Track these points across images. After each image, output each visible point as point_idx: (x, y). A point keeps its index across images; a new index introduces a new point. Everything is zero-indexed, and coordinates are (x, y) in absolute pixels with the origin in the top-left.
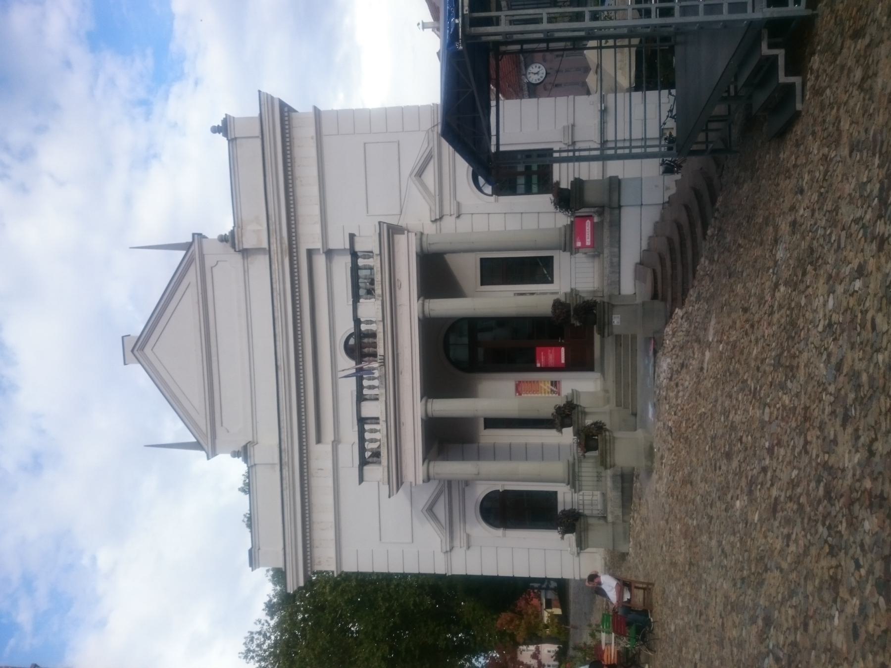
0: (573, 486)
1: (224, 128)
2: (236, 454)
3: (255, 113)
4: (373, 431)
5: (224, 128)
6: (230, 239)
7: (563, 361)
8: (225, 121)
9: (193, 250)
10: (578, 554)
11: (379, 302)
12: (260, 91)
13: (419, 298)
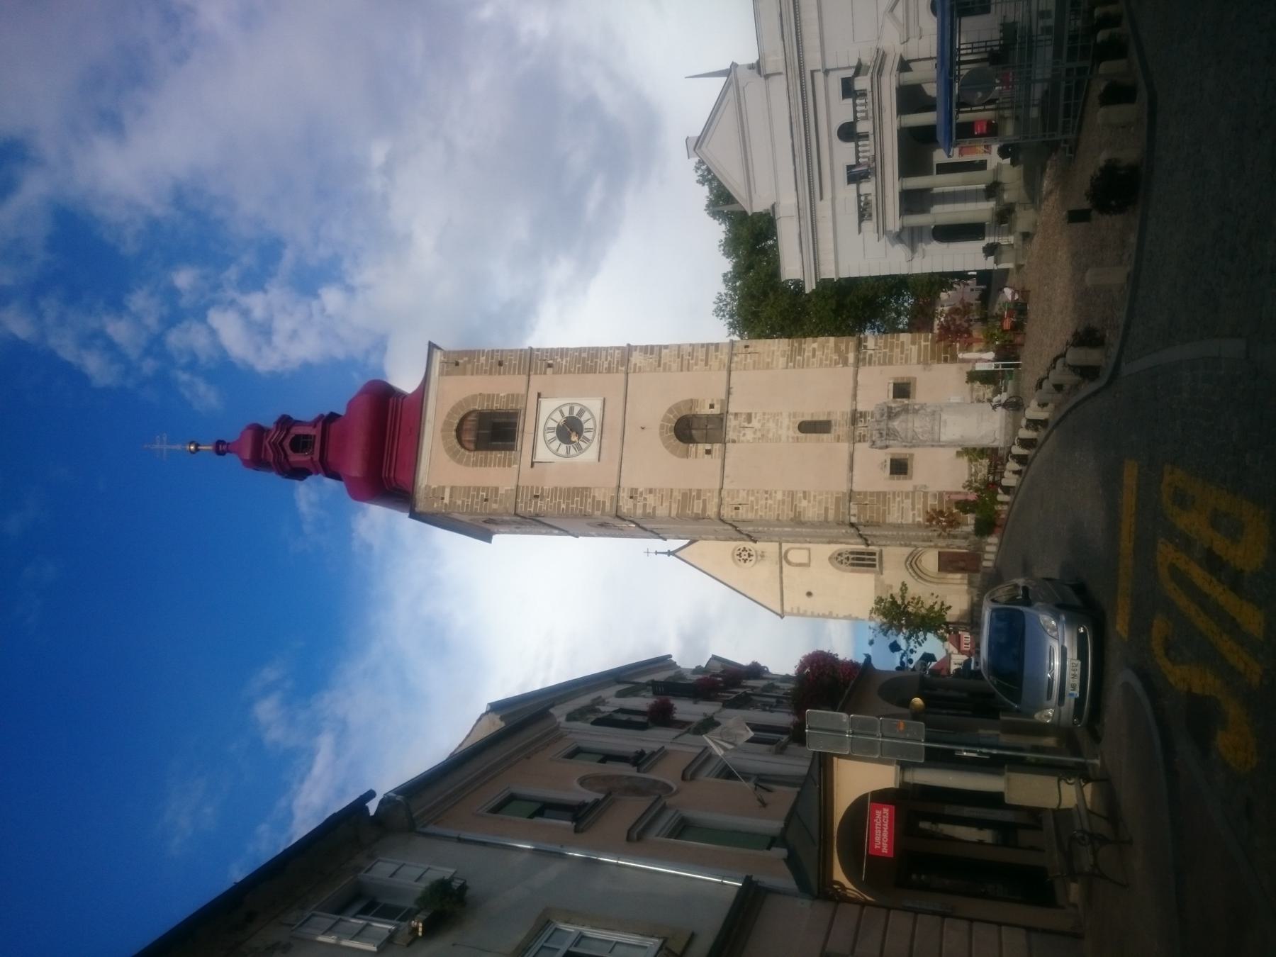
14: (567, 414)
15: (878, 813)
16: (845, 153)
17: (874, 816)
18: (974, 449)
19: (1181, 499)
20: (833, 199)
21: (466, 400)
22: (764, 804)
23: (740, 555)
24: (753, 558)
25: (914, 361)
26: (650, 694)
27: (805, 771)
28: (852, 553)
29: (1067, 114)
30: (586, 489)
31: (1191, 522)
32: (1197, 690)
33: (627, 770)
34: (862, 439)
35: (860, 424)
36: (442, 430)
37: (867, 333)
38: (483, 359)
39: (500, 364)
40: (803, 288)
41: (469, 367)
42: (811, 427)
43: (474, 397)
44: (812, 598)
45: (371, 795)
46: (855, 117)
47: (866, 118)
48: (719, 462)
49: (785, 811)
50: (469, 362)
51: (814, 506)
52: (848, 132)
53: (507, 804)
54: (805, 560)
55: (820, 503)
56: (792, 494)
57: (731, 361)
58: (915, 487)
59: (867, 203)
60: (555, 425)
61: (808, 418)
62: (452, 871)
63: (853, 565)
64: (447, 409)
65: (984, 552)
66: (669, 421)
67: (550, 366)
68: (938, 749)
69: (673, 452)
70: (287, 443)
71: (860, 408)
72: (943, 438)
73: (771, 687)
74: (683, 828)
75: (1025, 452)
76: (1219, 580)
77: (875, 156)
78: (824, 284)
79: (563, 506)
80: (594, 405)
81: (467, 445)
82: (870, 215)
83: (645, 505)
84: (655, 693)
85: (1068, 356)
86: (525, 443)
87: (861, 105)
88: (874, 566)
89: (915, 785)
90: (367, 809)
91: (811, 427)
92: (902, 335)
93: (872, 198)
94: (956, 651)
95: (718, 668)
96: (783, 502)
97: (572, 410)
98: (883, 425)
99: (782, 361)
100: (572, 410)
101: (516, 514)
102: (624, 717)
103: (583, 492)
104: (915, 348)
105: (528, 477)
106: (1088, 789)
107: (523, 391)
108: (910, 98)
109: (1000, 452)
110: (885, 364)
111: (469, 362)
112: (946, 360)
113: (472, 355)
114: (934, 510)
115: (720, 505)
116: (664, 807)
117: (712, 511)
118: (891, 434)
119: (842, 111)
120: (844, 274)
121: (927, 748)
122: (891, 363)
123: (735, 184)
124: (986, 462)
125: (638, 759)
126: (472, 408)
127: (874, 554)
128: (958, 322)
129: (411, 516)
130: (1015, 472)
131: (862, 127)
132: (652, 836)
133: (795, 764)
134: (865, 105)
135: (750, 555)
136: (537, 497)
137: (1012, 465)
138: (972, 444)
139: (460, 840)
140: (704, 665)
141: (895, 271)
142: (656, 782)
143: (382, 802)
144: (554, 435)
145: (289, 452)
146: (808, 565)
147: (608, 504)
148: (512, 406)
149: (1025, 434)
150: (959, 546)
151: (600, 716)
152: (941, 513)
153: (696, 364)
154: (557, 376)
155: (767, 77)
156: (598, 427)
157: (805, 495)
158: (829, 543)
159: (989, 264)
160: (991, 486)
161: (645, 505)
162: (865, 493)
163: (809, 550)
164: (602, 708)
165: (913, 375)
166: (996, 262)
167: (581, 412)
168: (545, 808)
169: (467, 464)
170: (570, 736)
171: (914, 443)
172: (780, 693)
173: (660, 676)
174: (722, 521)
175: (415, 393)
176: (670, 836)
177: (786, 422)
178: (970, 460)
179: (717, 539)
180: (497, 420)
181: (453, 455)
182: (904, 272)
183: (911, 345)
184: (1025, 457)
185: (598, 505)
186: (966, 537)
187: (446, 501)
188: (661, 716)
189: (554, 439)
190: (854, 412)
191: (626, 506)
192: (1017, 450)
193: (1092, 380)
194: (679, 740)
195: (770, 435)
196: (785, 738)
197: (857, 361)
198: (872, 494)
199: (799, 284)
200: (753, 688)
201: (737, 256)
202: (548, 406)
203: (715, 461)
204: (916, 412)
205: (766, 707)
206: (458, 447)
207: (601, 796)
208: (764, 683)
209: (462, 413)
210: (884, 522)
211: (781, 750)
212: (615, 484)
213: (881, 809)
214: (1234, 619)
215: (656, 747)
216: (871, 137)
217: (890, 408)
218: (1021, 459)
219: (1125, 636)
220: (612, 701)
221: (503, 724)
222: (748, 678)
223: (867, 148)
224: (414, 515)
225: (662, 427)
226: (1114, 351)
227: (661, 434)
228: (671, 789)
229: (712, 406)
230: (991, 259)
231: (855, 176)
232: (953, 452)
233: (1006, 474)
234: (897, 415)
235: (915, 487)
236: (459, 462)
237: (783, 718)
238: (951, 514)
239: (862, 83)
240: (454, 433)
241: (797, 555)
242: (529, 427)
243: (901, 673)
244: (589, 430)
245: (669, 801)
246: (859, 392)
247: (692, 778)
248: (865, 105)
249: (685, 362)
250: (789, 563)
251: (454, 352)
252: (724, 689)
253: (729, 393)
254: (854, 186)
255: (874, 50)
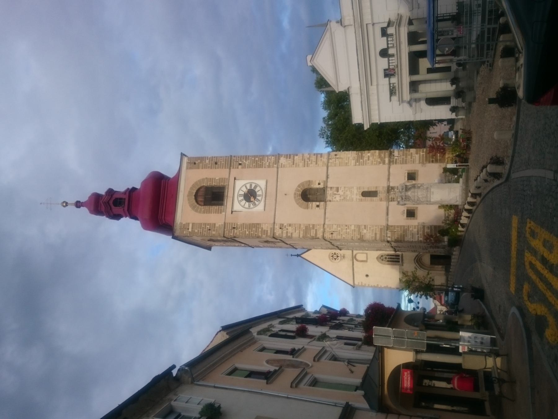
4: (392, 60)
10: (491, 101)
11: (395, 49)
14: (249, 188)
15: (406, 373)
16: (383, 63)
17: (404, 375)
18: (447, 205)
19: (533, 234)
20: (377, 85)
21: (199, 181)
22: (352, 372)
23: (333, 256)
24: (339, 258)
25: (418, 162)
26: (295, 323)
27: (371, 357)
28: (388, 255)
29: (488, 49)
30: (258, 224)
31: (536, 244)
32: (539, 313)
33: (289, 357)
34: (393, 200)
35: (392, 193)
36: (188, 196)
37: (394, 147)
38: (207, 161)
39: (216, 163)
40: (363, 128)
41: (201, 165)
42: (366, 194)
43: (203, 180)
44: (368, 278)
45: (174, 367)
46: (388, 46)
47: (393, 47)
48: (323, 211)
49: (362, 375)
50: (201, 162)
51: (369, 233)
52: (384, 53)
53: (233, 372)
54: (365, 259)
55: (373, 230)
56: (359, 227)
57: (328, 162)
58: (419, 223)
59: (394, 87)
60: (243, 193)
61: (366, 190)
62: (214, 400)
63: (388, 261)
64: (190, 186)
65: (452, 254)
66: (298, 191)
67: (240, 164)
68: (432, 344)
69: (301, 206)
70: (111, 202)
71: (392, 185)
72: (432, 200)
73: (351, 320)
74: (315, 383)
75: (471, 208)
76: (546, 268)
77: (397, 65)
78: (373, 125)
79: (247, 233)
80: (262, 183)
81: (200, 203)
82: (395, 93)
83: (287, 232)
84: (297, 323)
85: (488, 168)
86: (228, 202)
87: (391, 41)
88: (399, 262)
89: (422, 360)
90: (172, 373)
91: (366, 194)
92: (411, 149)
93: (396, 85)
94: (439, 304)
95: (325, 311)
96: (355, 230)
97: (251, 185)
98: (403, 194)
99: (353, 162)
100: (251, 185)
101: (224, 237)
102: (284, 333)
103: (256, 226)
104: (417, 156)
105: (230, 219)
106: (499, 360)
107: (227, 177)
108: (413, 38)
109: (460, 207)
110: (403, 163)
111: (201, 162)
112: (433, 162)
113: (202, 159)
114: (428, 235)
115: (324, 232)
116: (306, 374)
117: (320, 235)
118: (407, 198)
119: (382, 43)
120: (383, 121)
121: (428, 344)
122: (406, 163)
123: (329, 75)
124: (453, 211)
125: (293, 352)
126: (202, 185)
127: (398, 256)
128: (438, 144)
129: (173, 238)
130: (466, 217)
131: (391, 51)
132: (302, 385)
133: (367, 354)
134: (393, 40)
135: (337, 256)
136: (234, 228)
137: (465, 214)
138: (445, 203)
139: (215, 387)
140: (318, 310)
141: (408, 119)
142: (301, 362)
143: (179, 370)
144: (242, 198)
145: (113, 206)
146: (366, 261)
147: (269, 232)
148: (222, 184)
149: (470, 199)
150: (440, 252)
151: (273, 333)
152: (431, 236)
153: (311, 163)
154: (244, 169)
155: (345, 27)
156: (264, 194)
157: (365, 227)
158: (377, 250)
159: (453, 116)
160: (456, 221)
161: (287, 232)
162: (394, 226)
163: (367, 254)
164: (273, 329)
165: (416, 169)
166: (456, 115)
167: (256, 187)
168: (252, 374)
169: (200, 212)
170: (260, 342)
171: (419, 202)
172: (356, 323)
173: (299, 315)
174: (326, 240)
175: (174, 177)
176: (310, 386)
177: (355, 191)
178: (445, 210)
179: (322, 248)
180: (214, 191)
181: (194, 208)
182: (412, 120)
183: (416, 154)
184: (471, 210)
185: (264, 232)
186: (444, 247)
187: (190, 230)
188: (302, 333)
189: (242, 200)
190: (389, 187)
191: (278, 232)
192: (467, 207)
193: (499, 179)
194: (310, 344)
195: (348, 198)
196: (360, 343)
197: (390, 162)
198: (398, 226)
199: (361, 126)
200: (343, 320)
201: (330, 110)
202: (240, 184)
203: (320, 211)
204: (419, 187)
205: (350, 329)
206: (196, 204)
207: (277, 368)
208: (348, 318)
209: (198, 187)
210: (404, 241)
211: (359, 348)
212: (272, 222)
213: (407, 371)
214: (551, 284)
215: (301, 347)
216: (396, 56)
217: (406, 186)
218: (469, 211)
219: (513, 292)
220: (277, 326)
221: (228, 337)
222: (340, 316)
223: (394, 61)
224: (175, 237)
225: (295, 194)
226: (507, 167)
227: (295, 197)
228: (309, 365)
229: (319, 184)
230: (454, 114)
231: (388, 74)
232: (437, 206)
233: (462, 218)
234: (410, 189)
235: (419, 223)
236: (196, 211)
237: (359, 334)
238: (436, 237)
239: (391, 30)
240: (194, 197)
241: (361, 256)
242: (230, 194)
243: (414, 312)
244: (259, 196)
245: (308, 370)
246: (391, 177)
247: (318, 361)
248: (393, 40)
249: (306, 162)
250: (357, 260)
251: (193, 158)
252: (330, 321)
253: (327, 177)
254: (387, 79)
255: (396, 15)
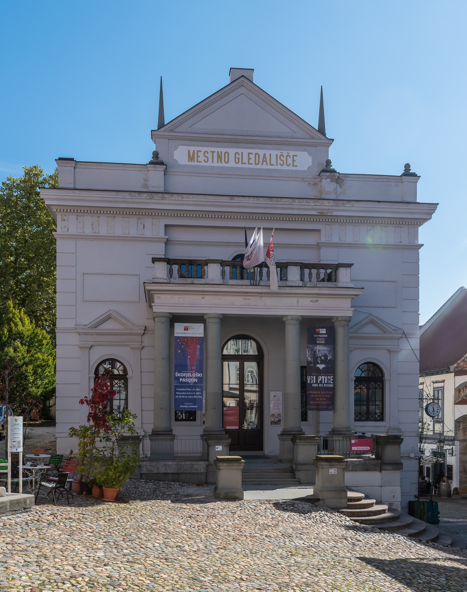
0: (282, 435)
1: (409, 174)
2: (156, 155)
3: (420, 199)
5: (409, 174)
6: (328, 169)
7: (228, 428)
8: (414, 175)
9: (319, 137)
12: (438, 204)
13: (301, 316)
